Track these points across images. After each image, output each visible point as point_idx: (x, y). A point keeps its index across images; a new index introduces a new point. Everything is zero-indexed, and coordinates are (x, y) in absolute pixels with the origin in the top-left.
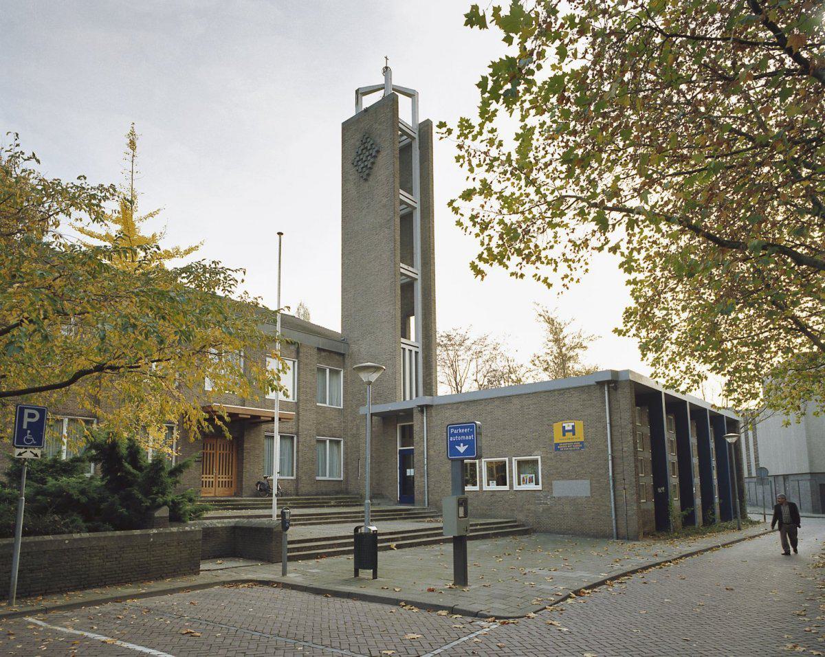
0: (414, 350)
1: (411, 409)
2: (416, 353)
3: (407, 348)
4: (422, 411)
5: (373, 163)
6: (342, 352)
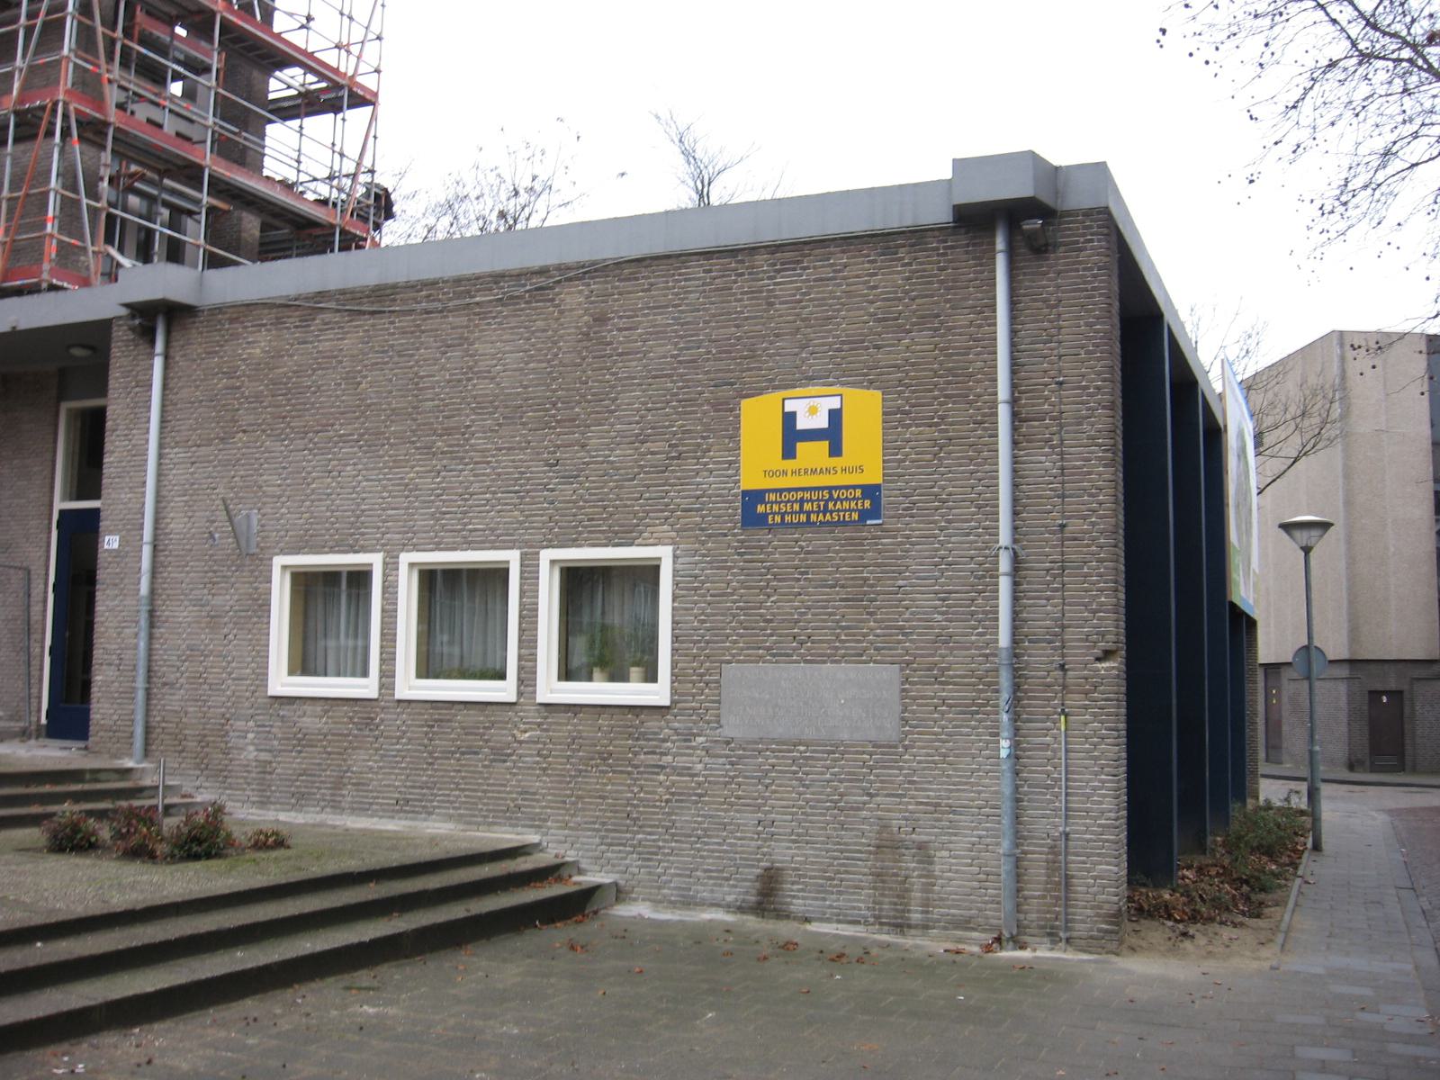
4: (148, 334)
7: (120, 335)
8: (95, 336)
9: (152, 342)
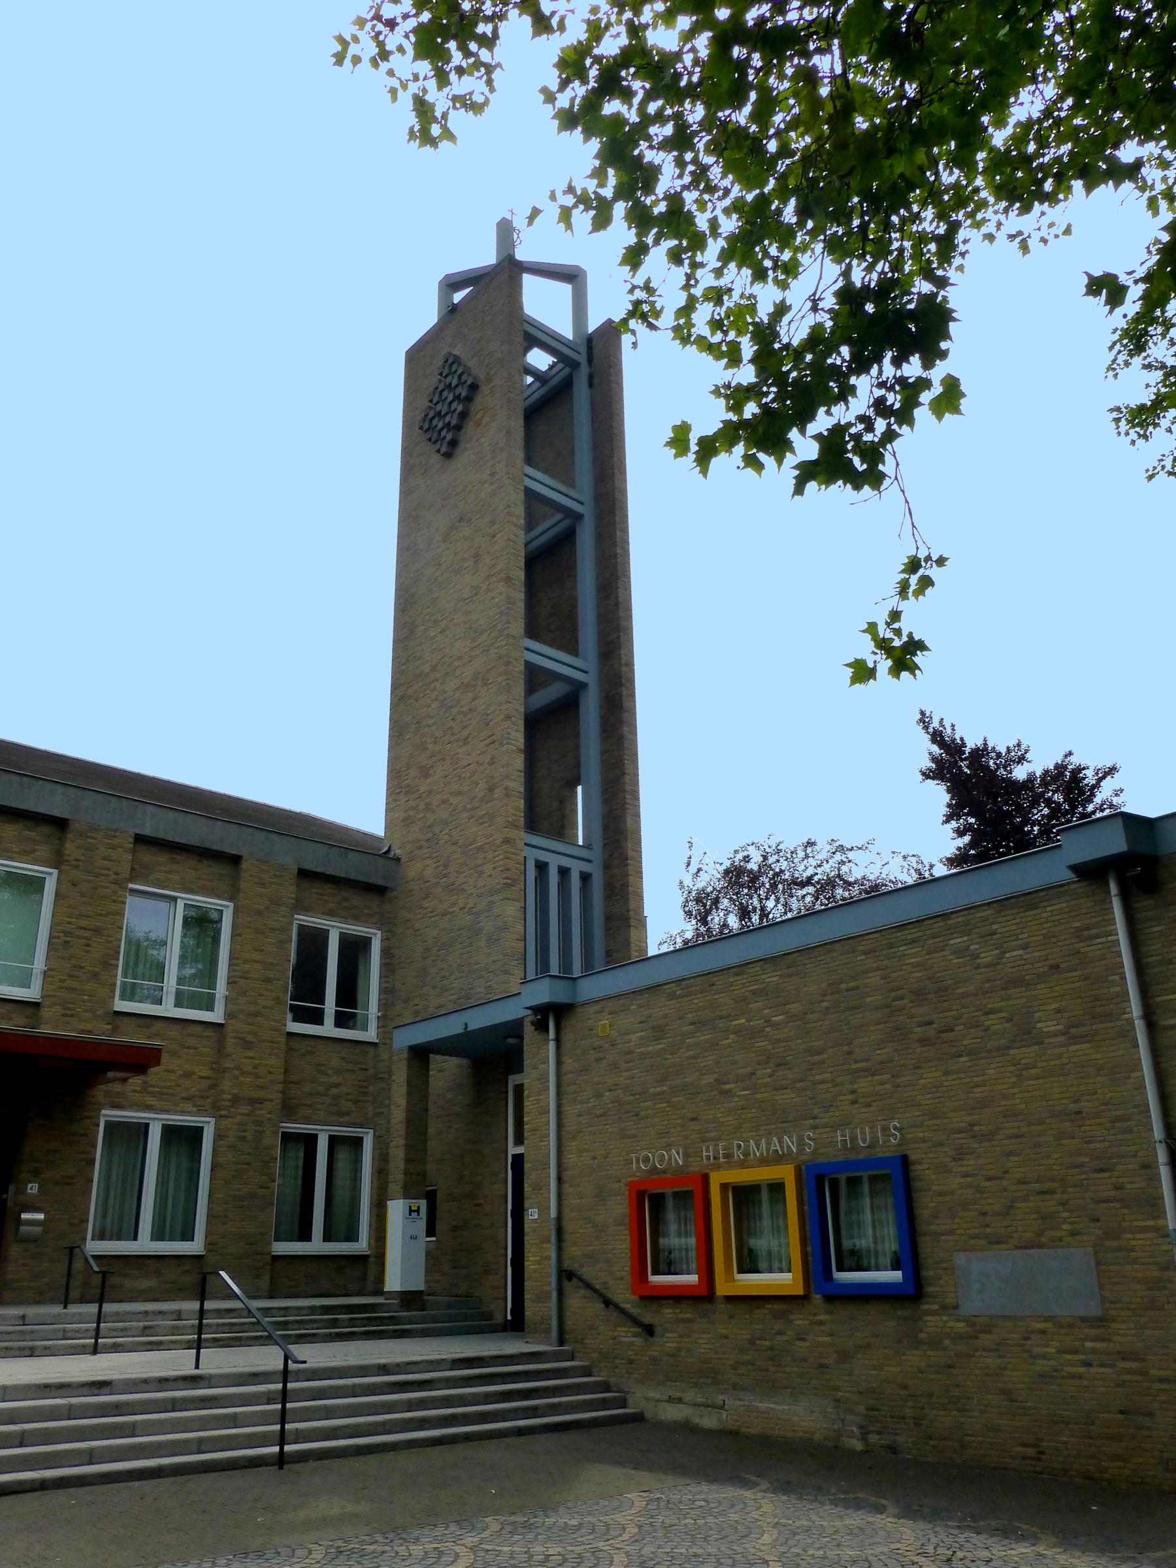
0: (576, 868)
1: (518, 1024)
2: (585, 878)
3: (554, 862)
4: (541, 1026)
5: (464, 415)
6: (380, 882)
7: (528, 1029)
8: (514, 1028)
9: (547, 1031)
